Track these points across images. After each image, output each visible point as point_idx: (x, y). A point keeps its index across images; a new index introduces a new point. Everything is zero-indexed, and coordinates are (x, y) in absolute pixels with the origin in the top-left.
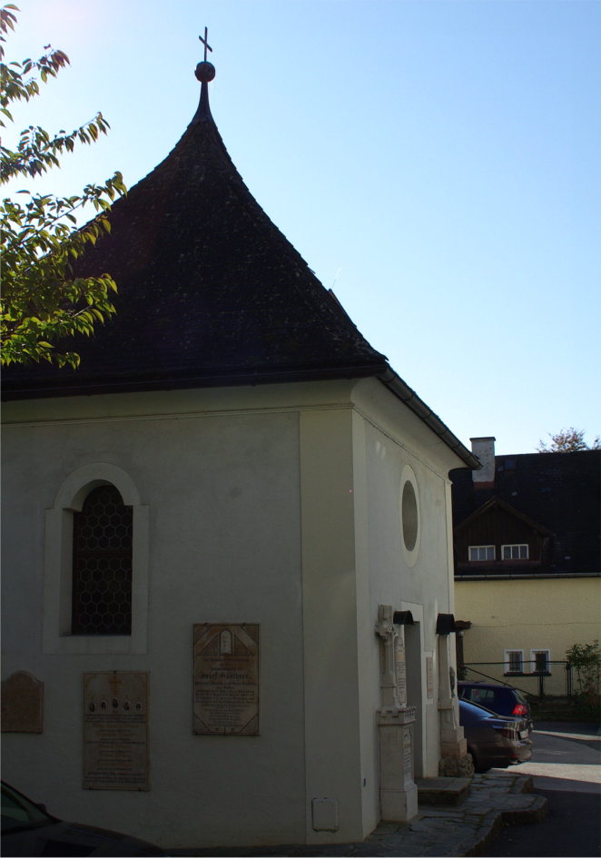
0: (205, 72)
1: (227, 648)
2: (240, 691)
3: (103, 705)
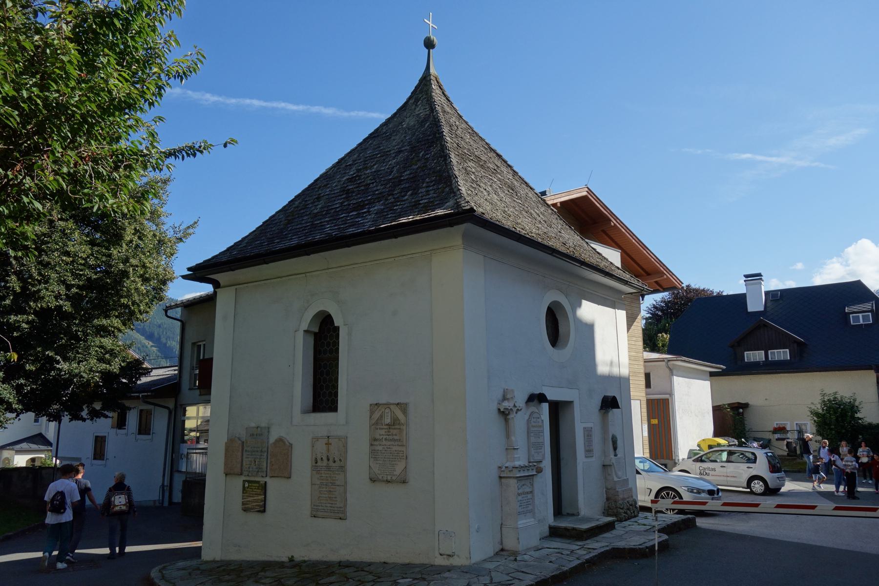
1: (388, 420)
2: (396, 451)
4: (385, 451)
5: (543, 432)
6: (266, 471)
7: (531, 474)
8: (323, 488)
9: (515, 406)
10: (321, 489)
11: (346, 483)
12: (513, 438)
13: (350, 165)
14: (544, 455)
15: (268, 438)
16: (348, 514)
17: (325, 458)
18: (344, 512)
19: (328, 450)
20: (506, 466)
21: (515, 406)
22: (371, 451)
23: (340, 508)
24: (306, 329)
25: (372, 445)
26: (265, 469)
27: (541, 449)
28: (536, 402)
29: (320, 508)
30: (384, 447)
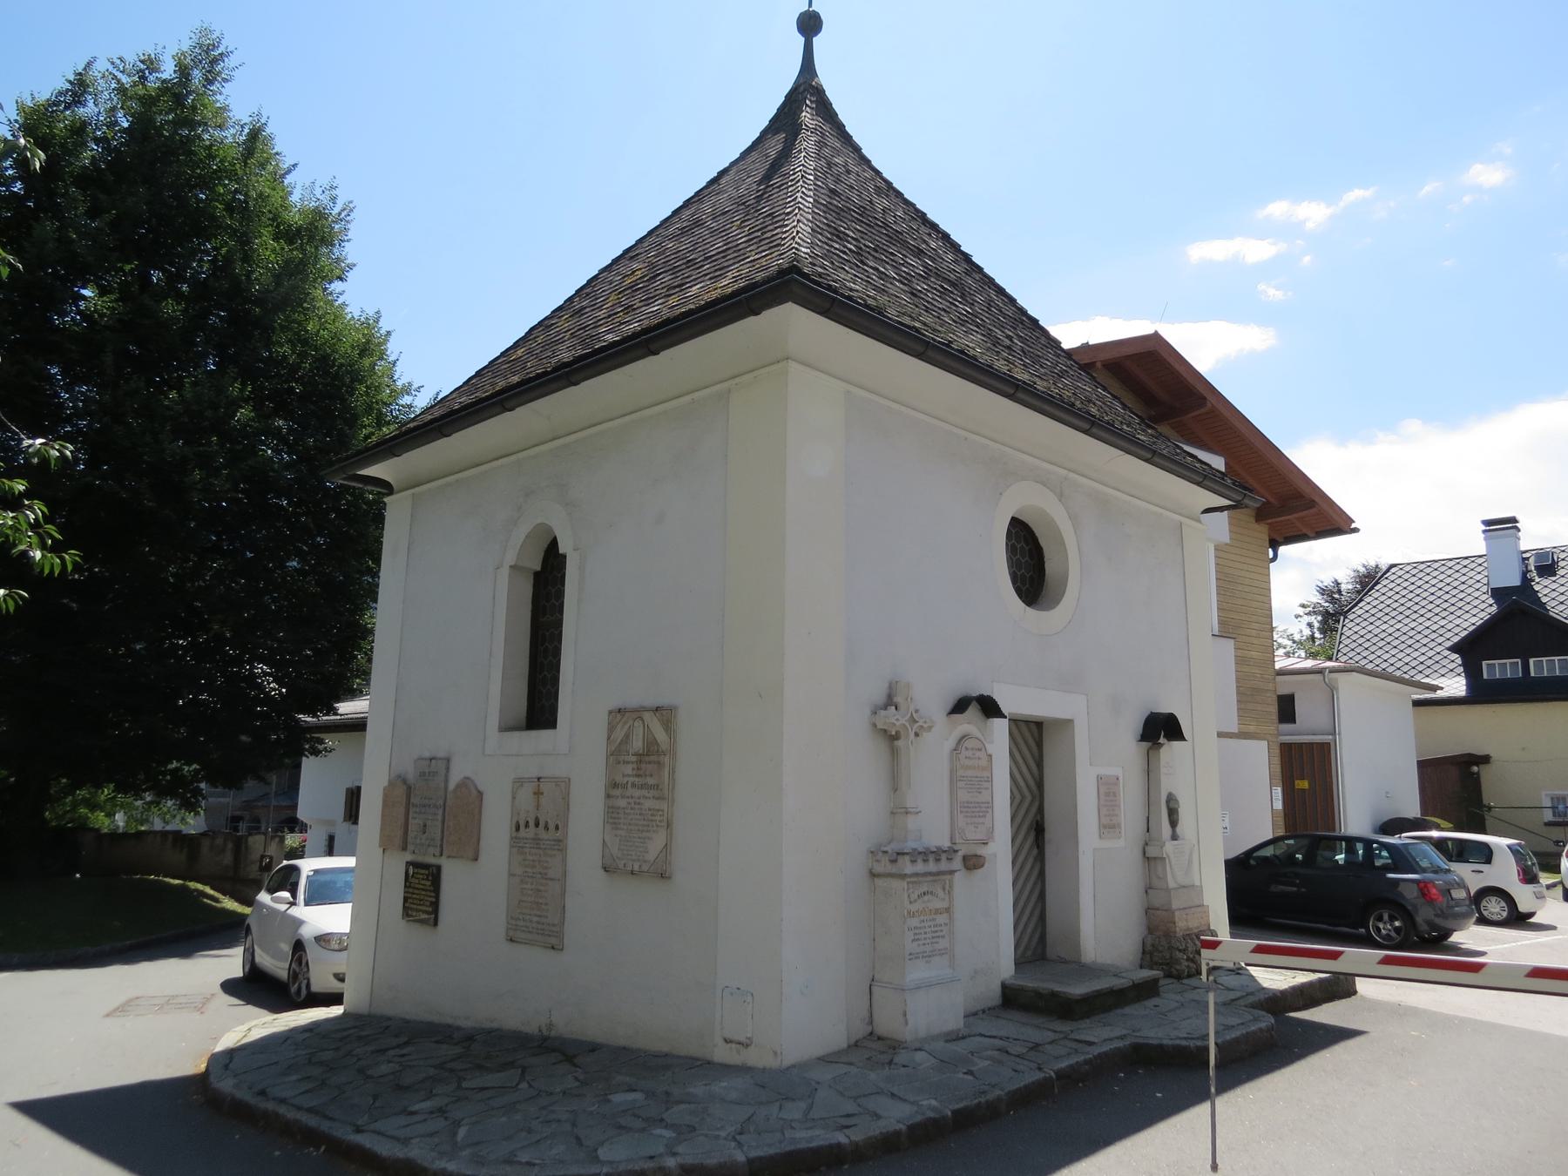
0: (810, 24)
1: (637, 744)
2: (650, 810)
3: (527, 825)
4: (632, 809)
5: (990, 780)
8: (527, 883)
10: (525, 886)
14: (991, 831)
17: (532, 824)
19: (538, 807)
23: (554, 925)
24: (513, 564)
25: (608, 796)
27: (985, 816)
28: (973, 711)
29: (521, 923)
30: (630, 800)
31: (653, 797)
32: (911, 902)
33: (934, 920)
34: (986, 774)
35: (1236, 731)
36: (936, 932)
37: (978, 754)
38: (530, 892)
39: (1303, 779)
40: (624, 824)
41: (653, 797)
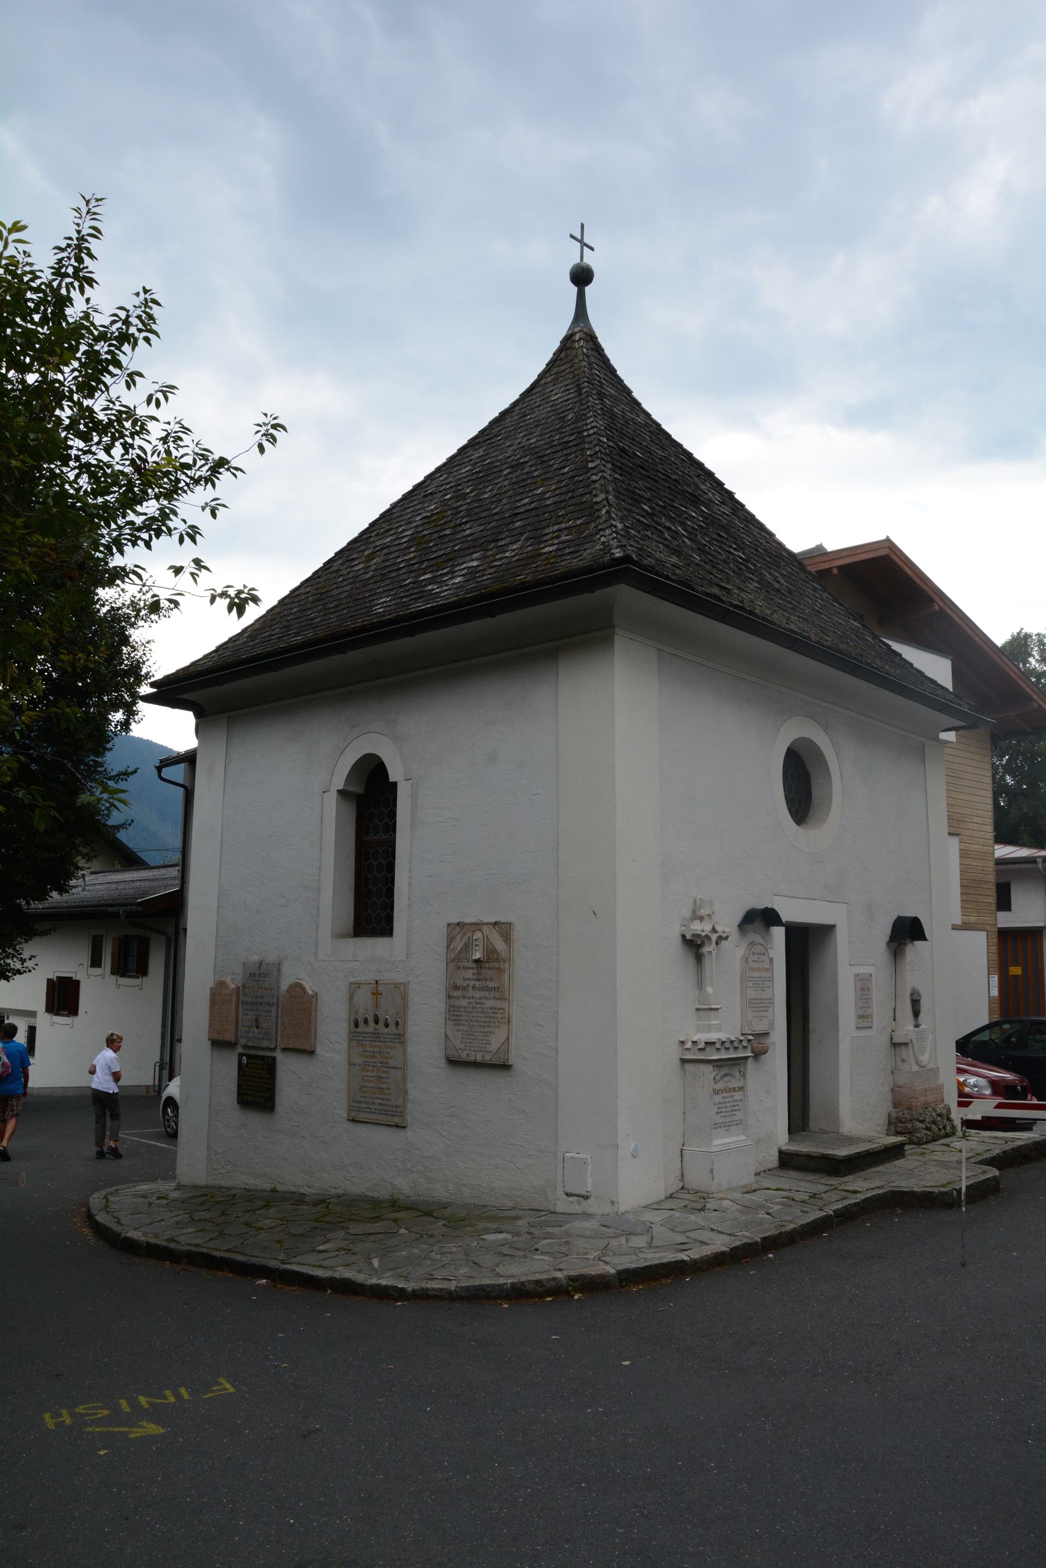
0: (582, 277)
2: (491, 1008)
3: (366, 1021)
5: (771, 980)
6: (276, 1039)
7: (743, 1055)
8: (368, 1071)
9: (714, 930)
10: (366, 1074)
11: (405, 1063)
12: (710, 990)
13: (431, 494)
14: (772, 1023)
15: (279, 982)
16: (409, 1118)
18: (402, 1115)
19: (377, 1006)
20: (694, 1040)
21: (714, 930)
22: (448, 1007)
23: (397, 1106)
24: (341, 788)
25: (449, 997)
26: (274, 1036)
27: (767, 1010)
28: (758, 925)
29: (364, 1105)
30: (471, 1000)
31: (494, 998)
32: (715, 1083)
33: (732, 1096)
34: (768, 974)
35: (960, 923)
36: (734, 1106)
37: (762, 958)
38: (372, 1079)
39: (1015, 965)
40: (466, 1021)
41: (494, 998)
